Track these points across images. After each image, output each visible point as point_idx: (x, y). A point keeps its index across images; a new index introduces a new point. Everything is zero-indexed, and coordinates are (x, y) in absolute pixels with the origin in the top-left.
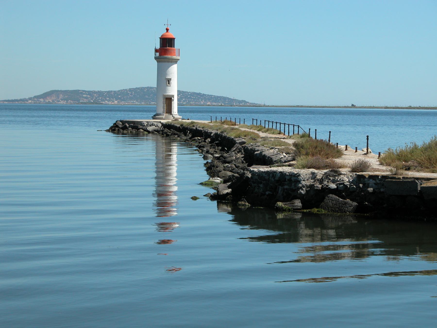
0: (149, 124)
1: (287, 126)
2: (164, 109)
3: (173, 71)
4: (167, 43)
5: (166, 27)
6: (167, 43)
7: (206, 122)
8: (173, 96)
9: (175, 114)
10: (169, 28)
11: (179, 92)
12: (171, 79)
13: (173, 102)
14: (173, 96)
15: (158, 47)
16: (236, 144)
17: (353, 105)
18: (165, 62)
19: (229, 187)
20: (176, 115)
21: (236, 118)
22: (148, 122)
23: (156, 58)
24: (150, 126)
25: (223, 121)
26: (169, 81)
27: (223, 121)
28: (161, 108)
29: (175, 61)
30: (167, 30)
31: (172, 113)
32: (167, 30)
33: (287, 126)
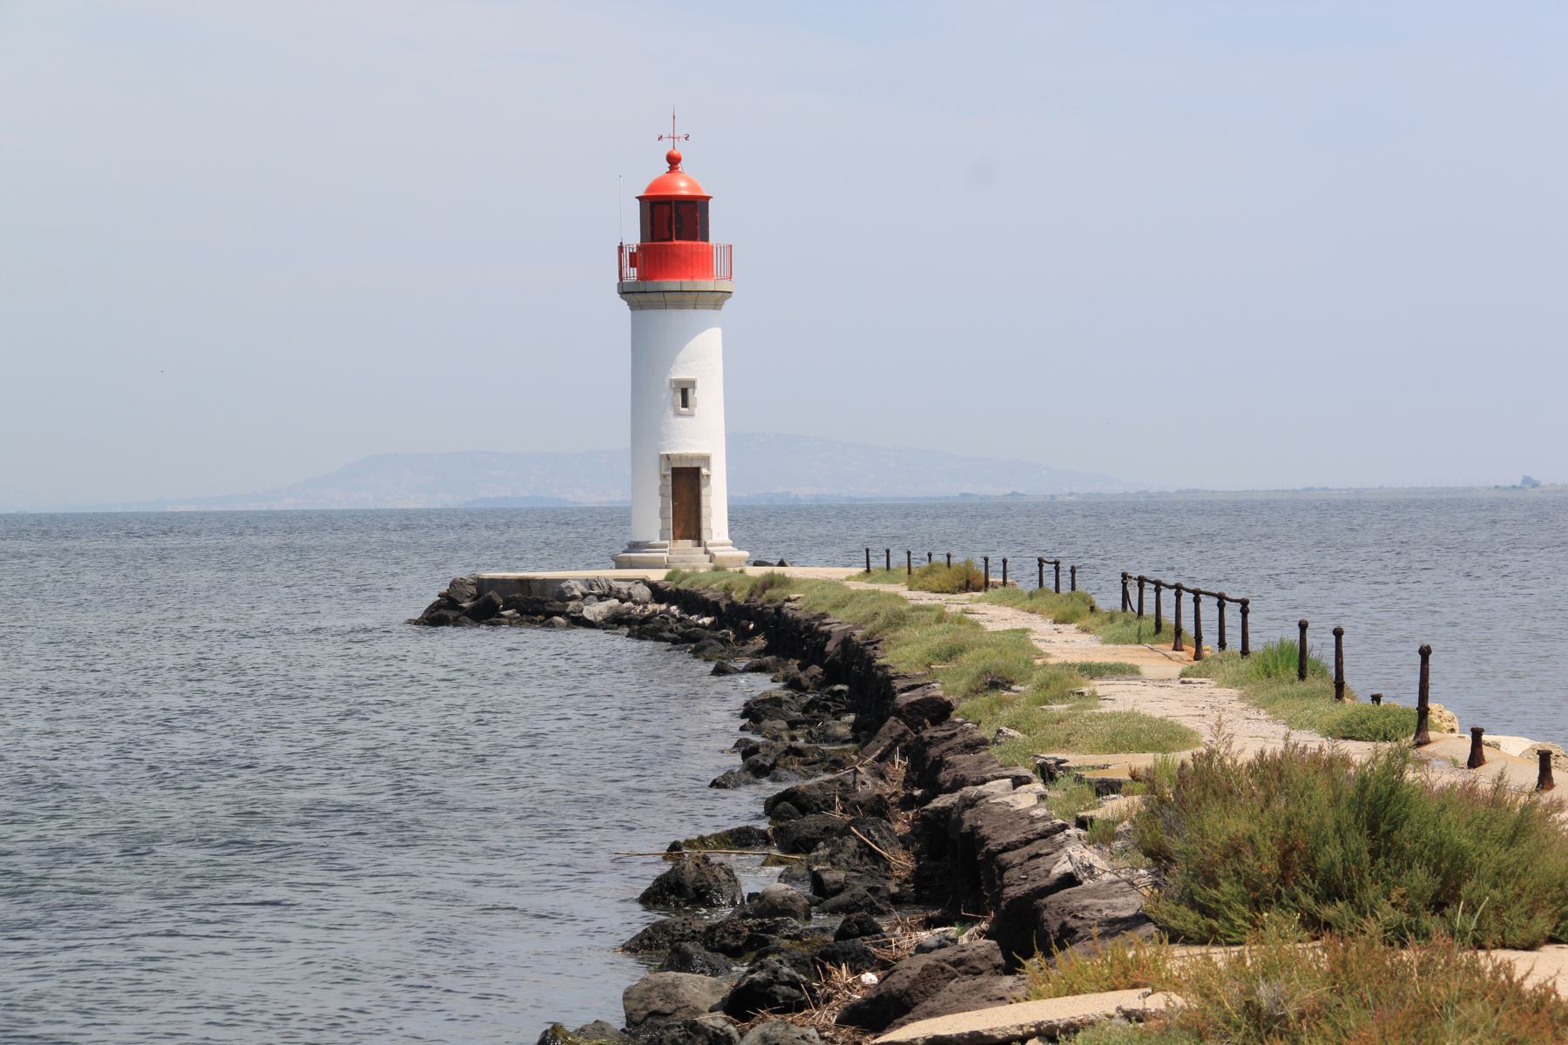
0: (596, 591)
1: (1187, 598)
2: (663, 518)
3: (703, 352)
4: (673, 225)
5: (666, 147)
6: (673, 225)
7: (837, 573)
8: (706, 459)
9: (716, 539)
10: (681, 149)
11: (736, 443)
12: (693, 383)
13: (704, 491)
14: (706, 459)
15: (633, 238)
16: (891, 720)
17: (1527, 480)
18: (664, 305)
19: (839, 967)
20: (721, 551)
21: (990, 556)
22: (590, 583)
23: (625, 292)
24: (600, 598)
25: (239, 660)
26: (685, 393)
27: (239, 660)
28: (651, 520)
29: (716, 299)
30: (673, 161)
31: (705, 536)
32: (673, 161)
33: (1187, 598)
